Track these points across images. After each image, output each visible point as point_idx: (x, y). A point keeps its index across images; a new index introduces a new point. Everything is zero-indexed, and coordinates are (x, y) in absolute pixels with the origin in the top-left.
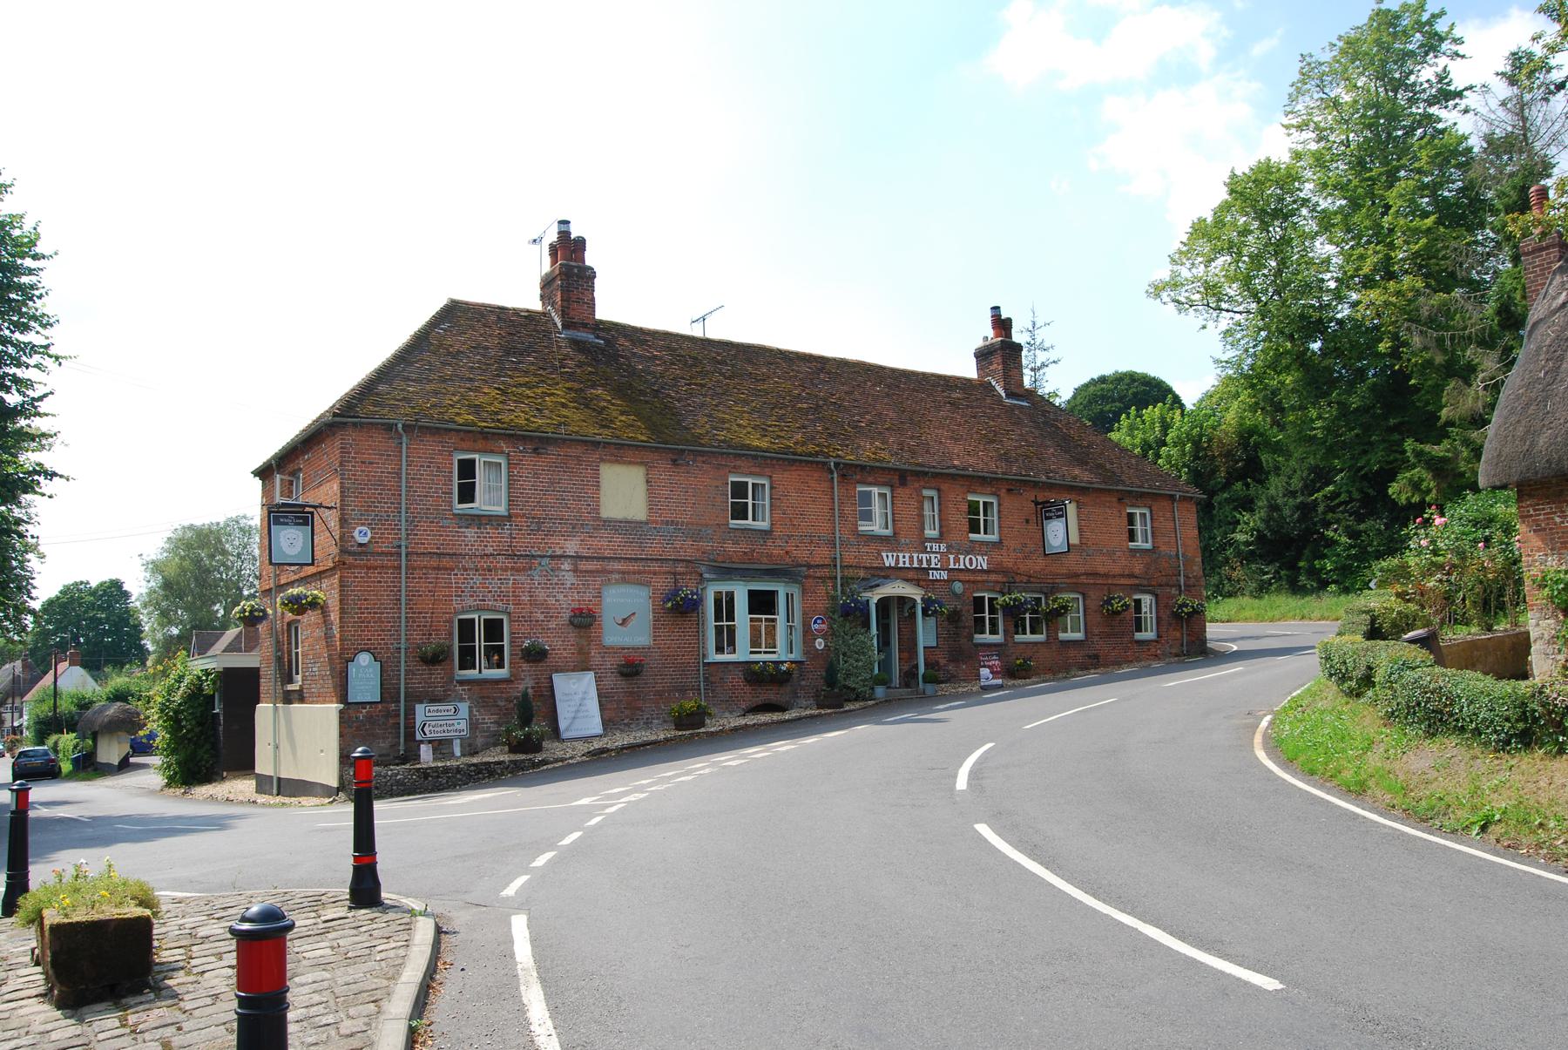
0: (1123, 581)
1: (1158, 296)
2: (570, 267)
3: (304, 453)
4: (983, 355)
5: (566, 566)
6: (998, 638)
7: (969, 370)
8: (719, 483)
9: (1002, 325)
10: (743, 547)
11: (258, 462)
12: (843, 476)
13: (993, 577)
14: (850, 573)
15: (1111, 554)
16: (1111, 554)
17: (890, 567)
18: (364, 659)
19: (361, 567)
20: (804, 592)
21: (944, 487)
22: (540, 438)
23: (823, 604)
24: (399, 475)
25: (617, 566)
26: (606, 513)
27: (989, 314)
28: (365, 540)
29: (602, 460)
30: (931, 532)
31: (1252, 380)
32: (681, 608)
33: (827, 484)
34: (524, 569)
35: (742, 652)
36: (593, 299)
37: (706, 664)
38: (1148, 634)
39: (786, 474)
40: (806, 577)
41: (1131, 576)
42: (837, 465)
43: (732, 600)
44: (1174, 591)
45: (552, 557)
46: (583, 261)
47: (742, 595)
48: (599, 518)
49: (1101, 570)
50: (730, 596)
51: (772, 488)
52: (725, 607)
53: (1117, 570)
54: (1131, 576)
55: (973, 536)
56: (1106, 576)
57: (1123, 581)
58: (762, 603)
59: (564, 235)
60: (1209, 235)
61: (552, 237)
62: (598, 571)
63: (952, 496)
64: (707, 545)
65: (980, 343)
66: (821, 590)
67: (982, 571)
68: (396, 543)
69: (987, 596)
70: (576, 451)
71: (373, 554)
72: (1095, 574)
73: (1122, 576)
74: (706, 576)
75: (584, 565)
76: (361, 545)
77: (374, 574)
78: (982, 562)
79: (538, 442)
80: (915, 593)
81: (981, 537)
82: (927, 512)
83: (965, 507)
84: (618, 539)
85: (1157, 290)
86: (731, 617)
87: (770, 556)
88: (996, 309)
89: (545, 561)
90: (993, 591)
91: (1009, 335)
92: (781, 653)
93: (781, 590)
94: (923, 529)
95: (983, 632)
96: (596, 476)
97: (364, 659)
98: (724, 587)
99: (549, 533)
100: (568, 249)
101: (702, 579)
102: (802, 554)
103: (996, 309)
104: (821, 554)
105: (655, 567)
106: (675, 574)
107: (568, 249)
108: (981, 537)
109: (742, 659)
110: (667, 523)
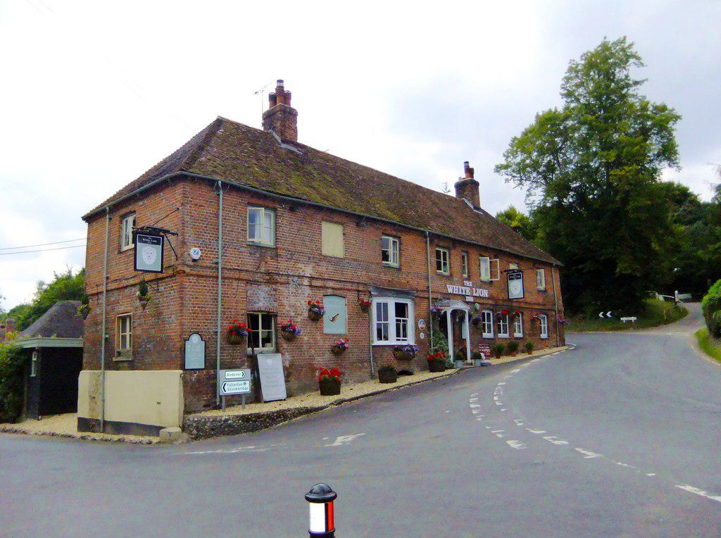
1: (498, 172)
2: (281, 109)
3: (140, 200)
4: (460, 187)
5: (306, 282)
6: (491, 335)
9: (470, 171)
10: (389, 278)
11: (89, 208)
12: (431, 241)
17: (450, 294)
18: (195, 339)
19: (193, 275)
20: (415, 304)
23: (424, 313)
24: (217, 216)
25: (330, 284)
28: (196, 257)
29: (323, 220)
30: (465, 276)
31: (707, 205)
35: (393, 341)
36: (296, 128)
38: (544, 336)
39: (407, 237)
41: (539, 304)
42: (429, 233)
45: (299, 276)
46: (290, 105)
47: (391, 302)
48: (321, 255)
50: (386, 305)
52: (383, 308)
53: (534, 301)
54: (539, 304)
56: (530, 304)
57: (537, 307)
58: (401, 310)
59: (280, 89)
60: (521, 144)
61: (272, 89)
62: (321, 287)
65: (456, 180)
66: (425, 303)
67: (485, 298)
68: (215, 260)
70: (310, 212)
71: (202, 267)
73: (535, 304)
74: (373, 293)
75: (316, 283)
76: (194, 260)
77: (202, 281)
78: (485, 293)
79: (294, 205)
80: (466, 308)
84: (331, 268)
85: (499, 168)
86: (386, 319)
87: (400, 284)
88: (280, 81)
89: (295, 279)
90: (490, 310)
91: (472, 177)
92: (410, 340)
93: (409, 303)
95: (485, 332)
96: (320, 228)
97: (195, 339)
98: (382, 300)
99: (297, 261)
100: (280, 97)
101: (371, 296)
102: (414, 283)
104: (422, 284)
105: (349, 286)
106: (359, 291)
107: (280, 97)
109: (393, 344)
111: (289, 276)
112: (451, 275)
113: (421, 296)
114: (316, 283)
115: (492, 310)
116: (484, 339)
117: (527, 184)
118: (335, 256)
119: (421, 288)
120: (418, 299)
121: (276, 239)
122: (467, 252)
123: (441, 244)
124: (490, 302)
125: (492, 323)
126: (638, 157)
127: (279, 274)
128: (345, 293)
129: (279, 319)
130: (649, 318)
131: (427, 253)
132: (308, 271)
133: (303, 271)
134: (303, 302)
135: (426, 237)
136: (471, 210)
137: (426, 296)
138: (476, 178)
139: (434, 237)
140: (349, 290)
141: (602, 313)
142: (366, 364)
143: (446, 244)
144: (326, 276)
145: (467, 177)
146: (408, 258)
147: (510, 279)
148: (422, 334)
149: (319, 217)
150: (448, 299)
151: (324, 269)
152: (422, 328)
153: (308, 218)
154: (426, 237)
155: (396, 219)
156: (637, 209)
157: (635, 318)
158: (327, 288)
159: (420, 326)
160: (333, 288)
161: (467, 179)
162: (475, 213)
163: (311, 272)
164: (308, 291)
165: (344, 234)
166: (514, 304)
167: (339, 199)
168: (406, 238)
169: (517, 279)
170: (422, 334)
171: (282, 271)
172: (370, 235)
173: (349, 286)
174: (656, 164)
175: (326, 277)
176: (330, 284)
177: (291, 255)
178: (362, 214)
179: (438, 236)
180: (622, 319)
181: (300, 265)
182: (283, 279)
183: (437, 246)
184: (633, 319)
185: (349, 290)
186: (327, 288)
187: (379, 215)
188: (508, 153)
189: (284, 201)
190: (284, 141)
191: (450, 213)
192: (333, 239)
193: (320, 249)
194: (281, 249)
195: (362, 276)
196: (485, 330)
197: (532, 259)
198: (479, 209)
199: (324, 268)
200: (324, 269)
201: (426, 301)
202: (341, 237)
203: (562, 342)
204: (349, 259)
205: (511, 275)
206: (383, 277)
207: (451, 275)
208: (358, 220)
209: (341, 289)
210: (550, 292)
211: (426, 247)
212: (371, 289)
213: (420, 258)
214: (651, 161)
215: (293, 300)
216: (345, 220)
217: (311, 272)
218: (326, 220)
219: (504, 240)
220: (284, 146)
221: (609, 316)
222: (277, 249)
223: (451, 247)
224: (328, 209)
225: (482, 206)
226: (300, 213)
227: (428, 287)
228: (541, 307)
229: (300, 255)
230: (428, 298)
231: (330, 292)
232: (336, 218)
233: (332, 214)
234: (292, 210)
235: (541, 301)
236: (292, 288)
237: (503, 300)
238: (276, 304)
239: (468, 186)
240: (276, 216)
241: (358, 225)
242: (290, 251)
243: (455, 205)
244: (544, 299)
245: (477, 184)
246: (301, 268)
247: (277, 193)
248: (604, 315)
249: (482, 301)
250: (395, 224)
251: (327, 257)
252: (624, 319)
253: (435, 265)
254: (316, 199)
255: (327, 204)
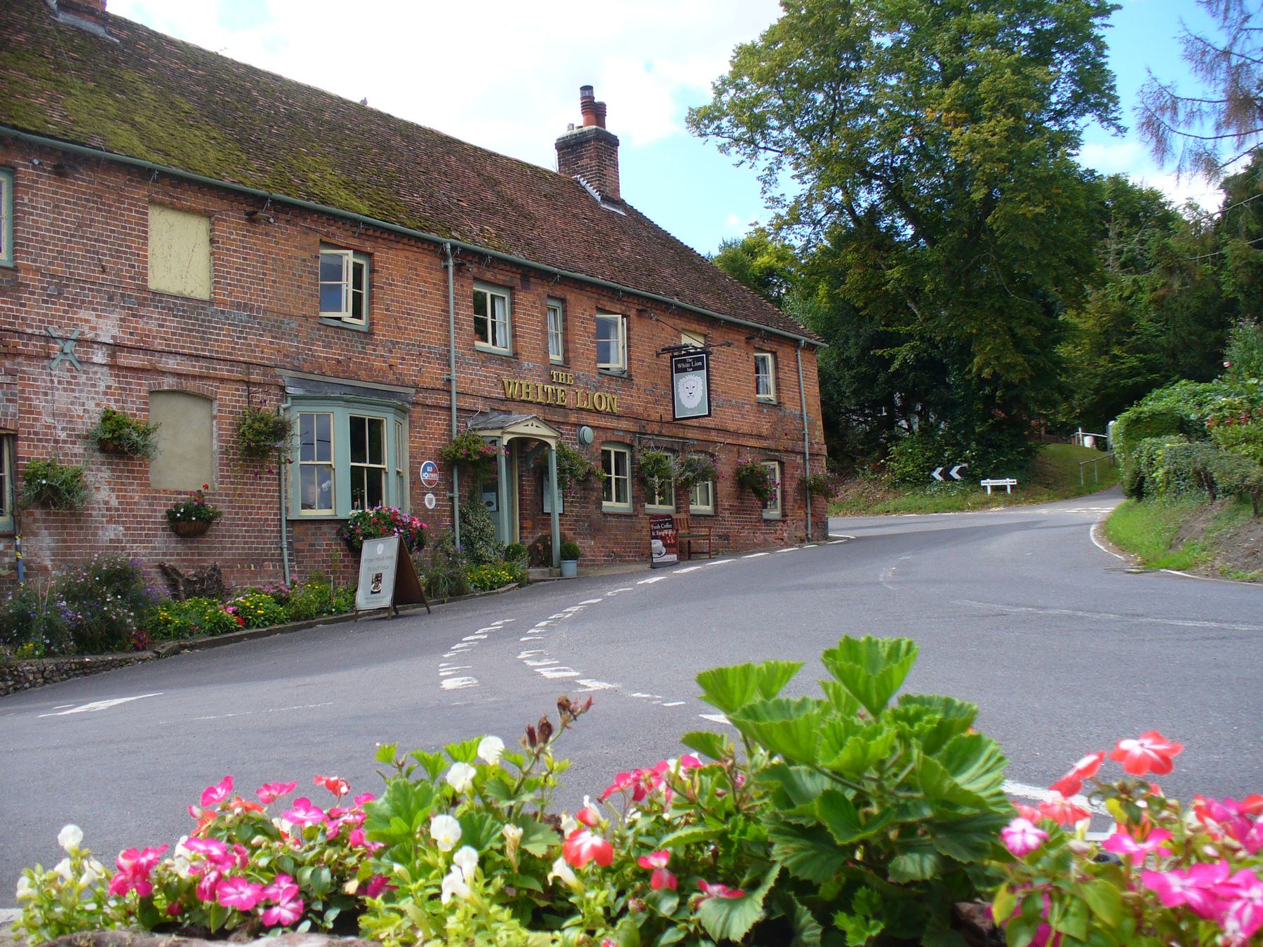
0: (752, 442)
4: (569, 148)
5: (100, 357)
6: (625, 507)
7: (548, 160)
8: (306, 255)
9: (594, 110)
10: (335, 353)
12: (459, 268)
13: (624, 424)
14: (467, 403)
15: (739, 407)
16: (739, 407)
21: (570, 297)
22: (65, 153)
25: (171, 363)
26: (153, 285)
27: (578, 95)
29: (153, 202)
30: (556, 357)
32: (257, 446)
33: (438, 275)
34: (38, 357)
37: (291, 523)
39: (391, 254)
40: (415, 404)
41: (759, 436)
42: (454, 248)
43: (354, 499)
44: (799, 460)
45: (79, 341)
48: (144, 289)
49: (732, 427)
51: (372, 271)
53: (746, 429)
54: (759, 436)
55: (479, 344)
56: (736, 434)
57: (752, 442)
62: (143, 370)
63: (579, 311)
64: (291, 345)
65: (563, 132)
69: (613, 450)
72: (724, 431)
75: (124, 359)
81: (487, 346)
82: (551, 330)
83: (592, 327)
84: (172, 323)
88: (587, 89)
89: (69, 347)
94: (547, 353)
95: (609, 499)
102: (408, 370)
103: (587, 89)
104: (432, 374)
105: (223, 371)
106: (248, 383)
108: (487, 346)
110: (238, 306)
111: (49, 338)
112: (516, 355)
113: (429, 402)
114: (124, 359)
115: (630, 446)
116: (605, 515)
117: (766, 158)
118: (186, 293)
119: (427, 382)
120: (419, 409)
121: (15, 244)
122: (563, 301)
123: (489, 276)
124: (624, 424)
125: (628, 477)
126: (1022, 101)
127: (21, 334)
128: (207, 387)
129: (23, 448)
130: (1041, 481)
131: (447, 297)
132: (108, 328)
133: (94, 328)
134: (91, 405)
135: (444, 256)
136: (594, 204)
137: (445, 403)
138: (611, 126)
139: (467, 259)
140: (222, 380)
141: (940, 469)
142: (269, 566)
143: (501, 278)
144: (158, 344)
145: (587, 123)
146: (415, 311)
147: (679, 371)
148: (430, 496)
149: (141, 193)
150: (505, 412)
151: (153, 325)
152: (429, 483)
153: (110, 197)
154: (444, 256)
155: (361, 209)
156: (1016, 222)
157: (1014, 482)
158: (163, 373)
159: (424, 476)
160: (179, 375)
161: (586, 129)
162: (604, 211)
163: (115, 332)
164: (105, 379)
165: (212, 241)
166: (690, 434)
167: (205, 153)
168: (391, 260)
169: (695, 369)
170: (430, 496)
171: (31, 326)
172: (287, 242)
173: (223, 371)
174: (1070, 123)
175: (159, 348)
176: (171, 363)
177: (59, 287)
178: (263, 192)
179: (480, 257)
180: (983, 483)
181: (83, 314)
182: (34, 347)
183: (477, 280)
184: (1008, 482)
185: (222, 380)
186: (163, 373)
187: (311, 196)
188: (723, 83)
189: (42, 150)
190: (606, 199)
191: (532, 207)
192: (179, 254)
193: (143, 276)
194: (28, 269)
195: (263, 346)
196: (610, 493)
197: (747, 327)
198: (621, 203)
199: (151, 323)
200: (153, 325)
201: (443, 415)
202: (203, 250)
203: (820, 532)
204: (224, 303)
205: (682, 361)
206: (320, 351)
207: (516, 355)
208: (256, 207)
209: (201, 377)
210: (791, 407)
211: (446, 281)
212: (286, 376)
213: (427, 308)
214: (1059, 115)
215: (62, 399)
216: (214, 204)
217: (115, 332)
218: (162, 205)
219: (727, 298)
220: (63, 18)
221: (957, 477)
222: (16, 269)
223: (517, 282)
224: (163, 175)
225: (626, 194)
226: (83, 181)
227: (449, 381)
228: (765, 444)
229: (83, 288)
230: (449, 409)
231: (168, 383)
232: (190, 200)
233: (180, 188)
234: (60, 172)
235: (765, 429)
236: (59, 371)
237: (661, 422)
238: (12, 409)
239: (592, 147)
240: (15, 187)
241: (252, 218)
242: (53, 276)
243: (546, 188)
244: (774, 426)
245: (613, 142)
246: (87, 321)
247: (15, 127)
248: (946, 475)
249: (602, 422)
250: (355, 222)
251: (162, 295)
252: (988, 483)
253: (469, 327)
254: (125, 142)
255: (154, 160)
